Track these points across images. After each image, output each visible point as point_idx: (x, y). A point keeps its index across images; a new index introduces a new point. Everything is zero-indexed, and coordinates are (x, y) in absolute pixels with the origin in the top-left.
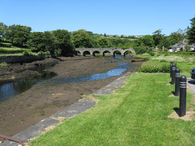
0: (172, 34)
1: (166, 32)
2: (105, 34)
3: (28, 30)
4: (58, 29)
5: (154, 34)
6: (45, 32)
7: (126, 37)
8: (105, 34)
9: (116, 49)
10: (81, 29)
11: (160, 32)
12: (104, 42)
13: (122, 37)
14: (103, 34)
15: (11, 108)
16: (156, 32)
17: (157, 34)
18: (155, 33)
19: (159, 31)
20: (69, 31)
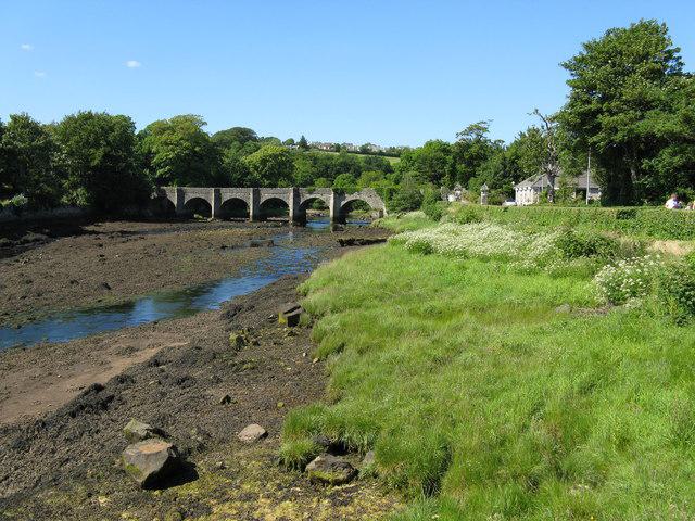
0: (522, 135)
1: (505, 132)
2: (303, 138)
3: (576, 431)
4: (85, 109)
5: (460, 137)
6: (15, 119)
7: (381, 153)
8: (303, 138)
9: (310, 193)
10: (183, 112)
11: (485, 130)
12: (281, 165)
13: (365, 150)
14: (297, 140)
15: (72, 283)
16: (470, 130)
17: (473, 137)
18: (463, 133)
19: (479, 129)
20: (451, 139)
